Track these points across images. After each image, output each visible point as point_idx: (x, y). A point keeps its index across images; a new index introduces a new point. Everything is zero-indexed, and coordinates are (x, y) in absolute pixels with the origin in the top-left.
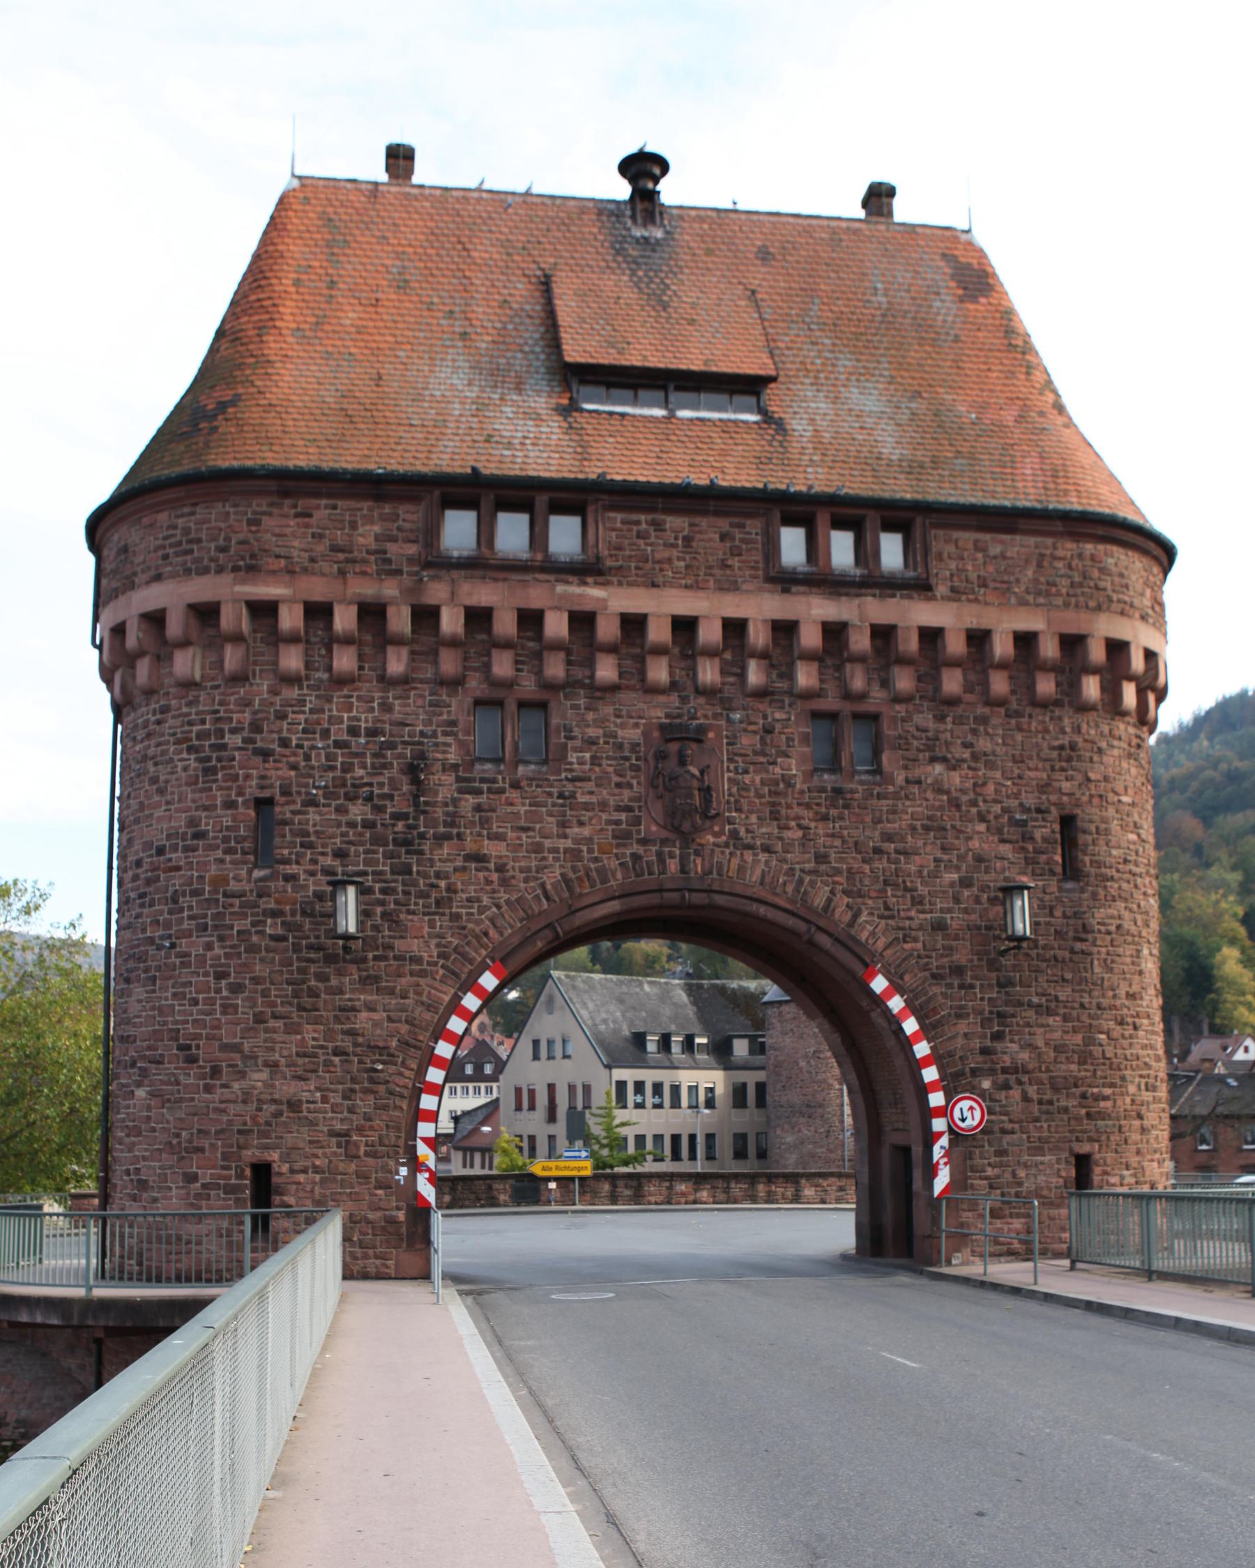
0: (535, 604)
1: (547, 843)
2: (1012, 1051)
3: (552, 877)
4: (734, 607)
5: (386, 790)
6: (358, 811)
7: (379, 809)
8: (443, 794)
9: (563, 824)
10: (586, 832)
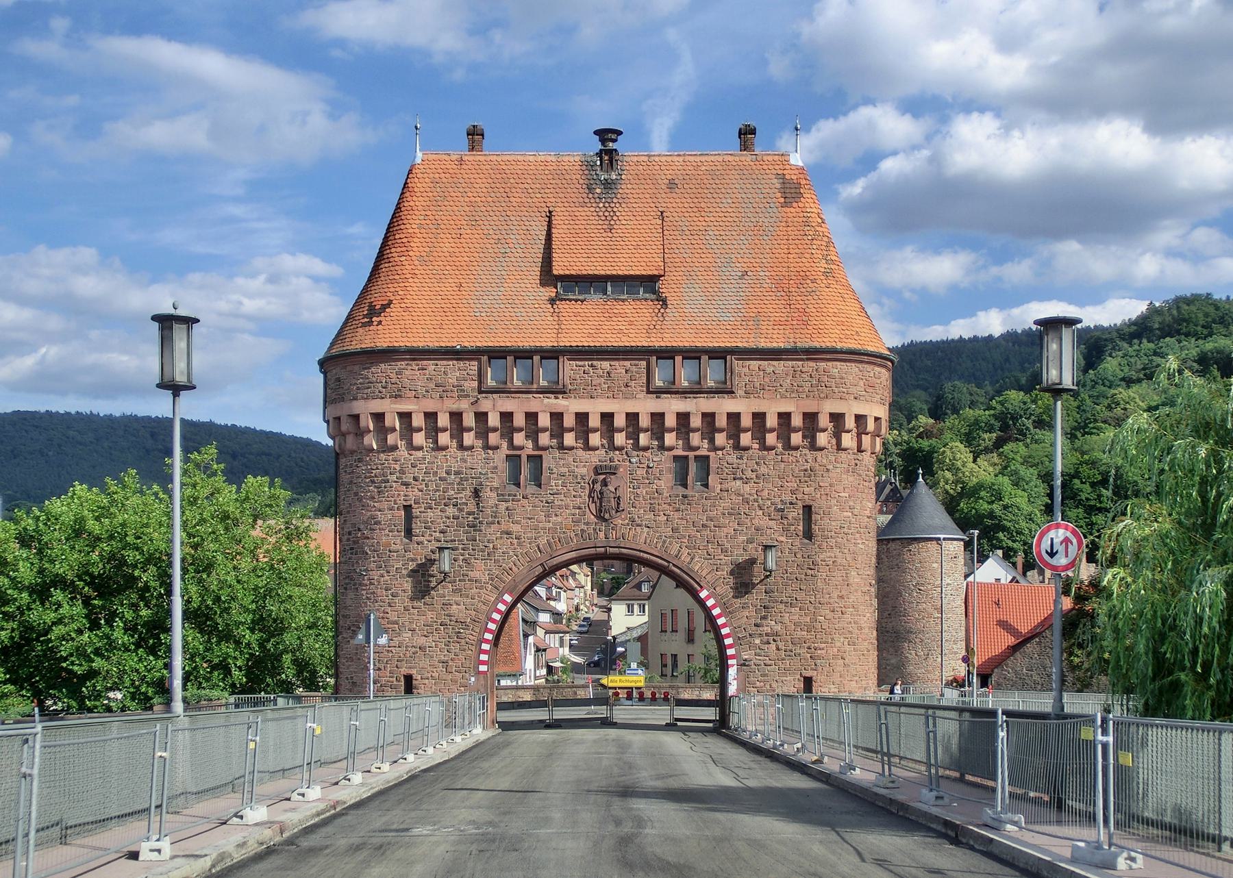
0: (533, 410)
1: (541, 525)
2: (770, 625)
3: (543, 542)
4: (632, 407)
5: (464, 500)
6: (451, 511)
7: (461, 510)
8: (491, 502)
9: (547, 516)
10: (559, 519)
